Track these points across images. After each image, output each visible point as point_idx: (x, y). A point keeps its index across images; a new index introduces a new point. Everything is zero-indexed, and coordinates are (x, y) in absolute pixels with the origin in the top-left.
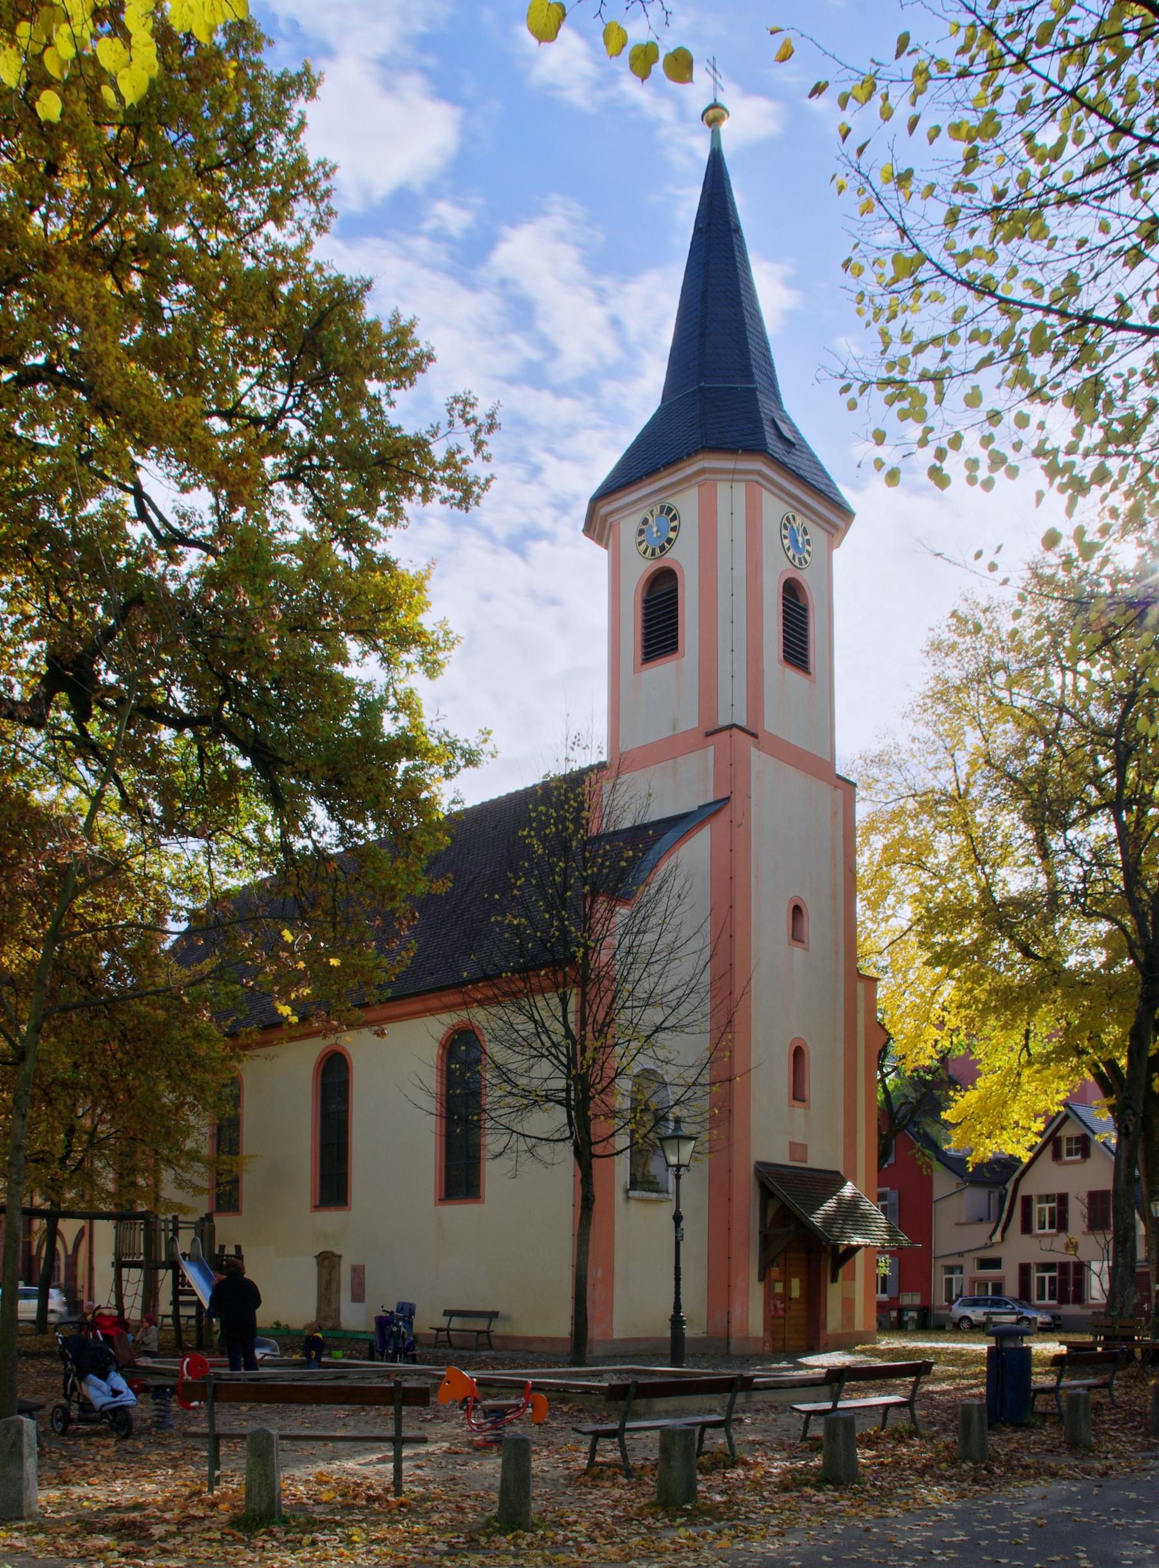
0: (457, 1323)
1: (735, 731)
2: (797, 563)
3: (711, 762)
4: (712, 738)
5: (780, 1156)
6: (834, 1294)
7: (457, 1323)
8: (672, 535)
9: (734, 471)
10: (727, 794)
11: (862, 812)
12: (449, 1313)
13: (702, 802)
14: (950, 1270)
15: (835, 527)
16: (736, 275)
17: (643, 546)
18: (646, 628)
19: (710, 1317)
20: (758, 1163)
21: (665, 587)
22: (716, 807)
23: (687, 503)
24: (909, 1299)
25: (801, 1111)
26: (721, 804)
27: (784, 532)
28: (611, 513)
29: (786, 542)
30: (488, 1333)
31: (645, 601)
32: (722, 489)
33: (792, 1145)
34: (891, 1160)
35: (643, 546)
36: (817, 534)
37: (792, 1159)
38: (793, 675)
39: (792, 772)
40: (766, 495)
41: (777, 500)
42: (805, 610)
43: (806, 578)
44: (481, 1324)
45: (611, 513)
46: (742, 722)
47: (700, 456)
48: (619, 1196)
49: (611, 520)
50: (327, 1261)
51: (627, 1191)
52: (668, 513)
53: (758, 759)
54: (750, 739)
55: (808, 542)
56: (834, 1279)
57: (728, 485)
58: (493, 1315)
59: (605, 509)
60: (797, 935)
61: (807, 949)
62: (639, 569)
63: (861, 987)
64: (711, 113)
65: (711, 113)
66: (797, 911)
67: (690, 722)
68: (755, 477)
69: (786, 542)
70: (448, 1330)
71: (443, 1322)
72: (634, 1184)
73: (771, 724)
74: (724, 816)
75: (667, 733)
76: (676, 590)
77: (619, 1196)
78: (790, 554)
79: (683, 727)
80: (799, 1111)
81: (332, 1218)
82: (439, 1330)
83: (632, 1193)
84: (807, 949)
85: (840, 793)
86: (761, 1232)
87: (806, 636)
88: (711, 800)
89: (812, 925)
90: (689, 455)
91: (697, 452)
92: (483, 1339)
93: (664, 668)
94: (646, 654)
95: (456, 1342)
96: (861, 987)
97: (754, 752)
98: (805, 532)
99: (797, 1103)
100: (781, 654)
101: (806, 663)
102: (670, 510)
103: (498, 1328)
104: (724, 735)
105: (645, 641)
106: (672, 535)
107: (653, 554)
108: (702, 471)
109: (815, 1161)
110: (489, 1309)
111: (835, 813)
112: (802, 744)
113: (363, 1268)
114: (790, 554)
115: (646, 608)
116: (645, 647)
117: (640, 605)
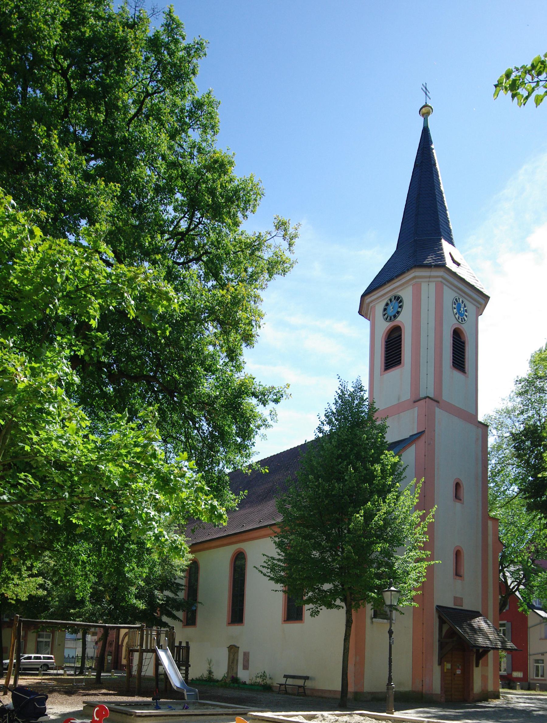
0: (290, 681)
1: (427, 399)
2: (460, 320)
3: (416, 415)
4: (417, 403)
5: (449, 603)
6: (477, 673)
7: (290, 681)
8: (399, 310)
9: (430, 277)
10: (424, 429)
11: (492, 441)
12: (286, 676)
13: (411, 434)
14: (537, 661)
15: (480, 304)
16: (434, 186)
17: (386, 316)
18: (386, 354)
19: (413, 679)
20: (437, 606)
21: (396, 334)
22: (418, 435)
23: (407, 295)
24: (517, 674)
25: (460, 581)
26: (419, 435)
27: (454, 306)
28: (372, 302)
29: (455, 311)
30: (303, 687)
31: (386, 342)
32: (424, 286)
33: (455, 598)
34: (507, 608)
35: (386, 316)
36: (471, 308)
37: (455, 605)
38: (457, 374)
39: (388, 660)
40: (445, 288)
41: (451, 291)
42: (464, 343)
43: (465, 328)
44: (300, 682)
45: (372, 302)
46: (432, 396)
47: (413, 270)
48: (368, 620)
49: (371, 305)
50: (233, 650)
51: (372, 619)
52: (398, 300)
53: (440, 414)
54: (435, 403)
55: (466, 311)
56: (477, 666)
57: (427, 284)
58: (306, 678)
59: (368, 299)
60: (457, 497)
61: (463, 504)
62: (384, 326)
63: (490, 523)
64: (424, 110)
65: (424, 110)
66: (458, 486)
67: (407, 396)
68: (440, 279)
69: (455, 311)
70: (285, 685)
71: (283, 681)
72: (375, 616)
73: (446, 397)
74: (423, 438)
75: (395, 402)
76: (401, 335)
77: (368, 620)
78: (457, 316)
79: (403, 399)
80: (459, 582)
81: (236, 629)
82: (281, 685)
83: (374, 620)
84: (463, 504)
85: (480, 430)
86: (439, 641)
87: (464, 356)
88: (416, 432)
89: (466, 492)
90: (408, 270)
91: (411, 268)
92: (301, 690)
93: (395, 372)
94: (386, 366)
95: (289, 691)
96: (490, 523)
97: (437, 410)
98: (465, 306)
99: (458, 578)
100: (452, 364)
101: (464, 368)
102: (399, 298)
103: (309, 684)
104: (422, 402)
105: (386, 360)
106: (399, 310)
107: (390, 319)
108: (414, 278)
109: (467, 606)
110: (305, 675)
111: (477, 439)
112: (461, 406)
113: (249, 653)
114: (457, 316)
115: (386, 345)
116: (386, 363)
117: (384, 343)
